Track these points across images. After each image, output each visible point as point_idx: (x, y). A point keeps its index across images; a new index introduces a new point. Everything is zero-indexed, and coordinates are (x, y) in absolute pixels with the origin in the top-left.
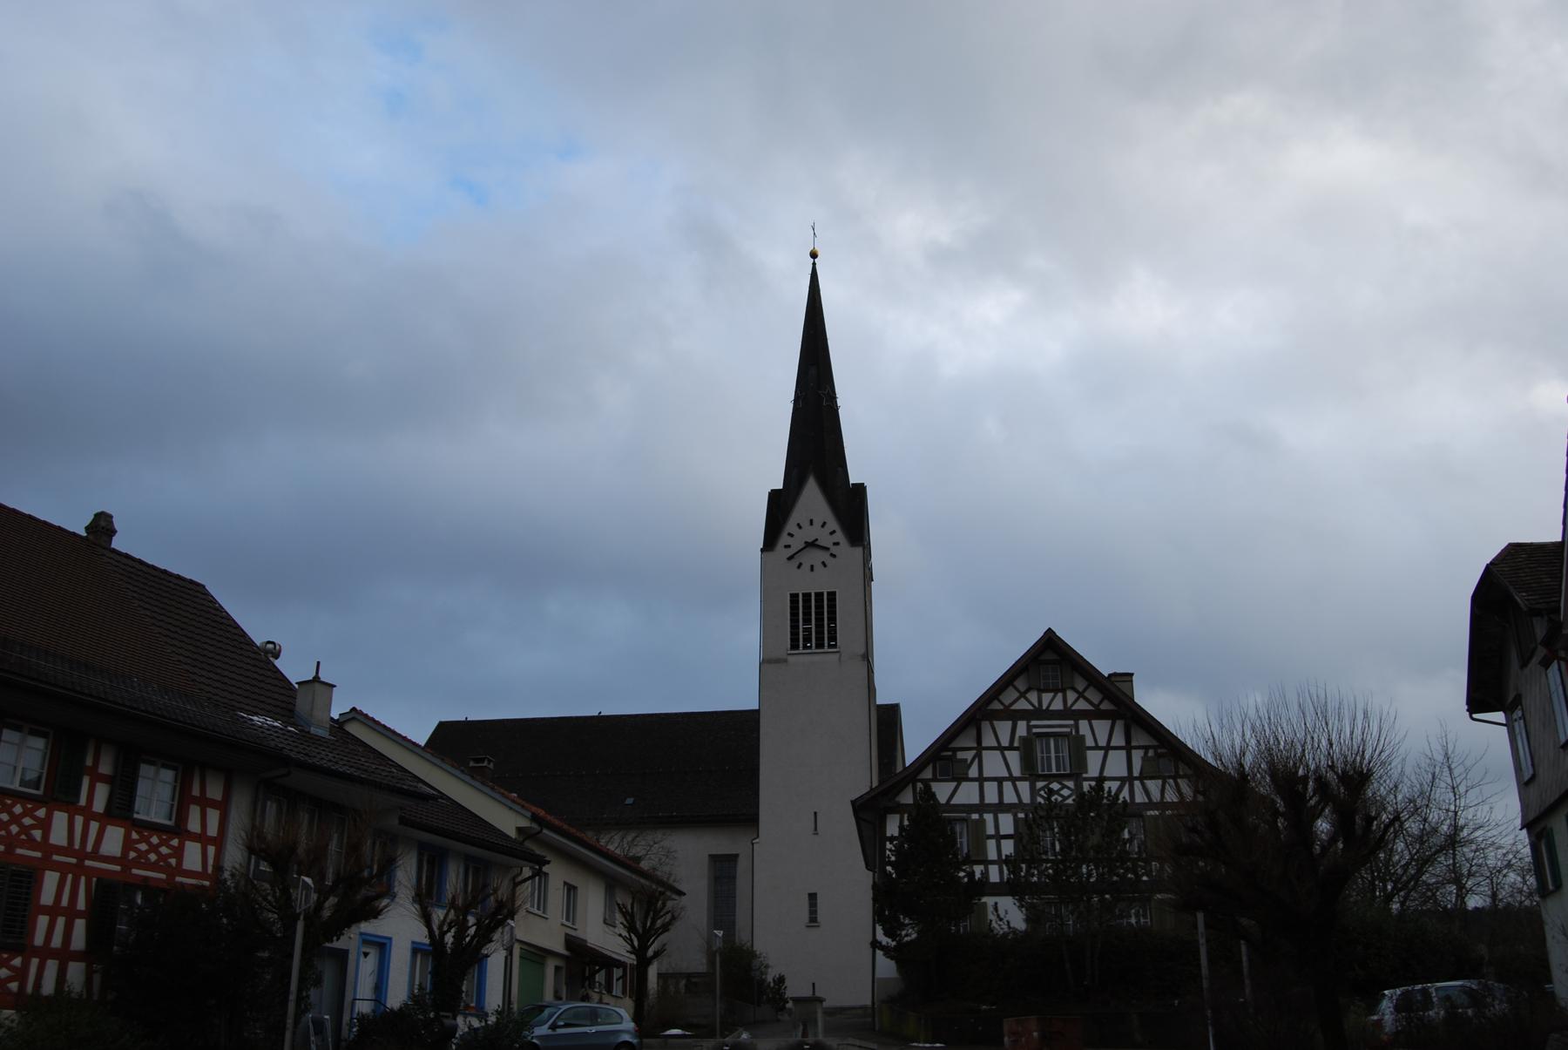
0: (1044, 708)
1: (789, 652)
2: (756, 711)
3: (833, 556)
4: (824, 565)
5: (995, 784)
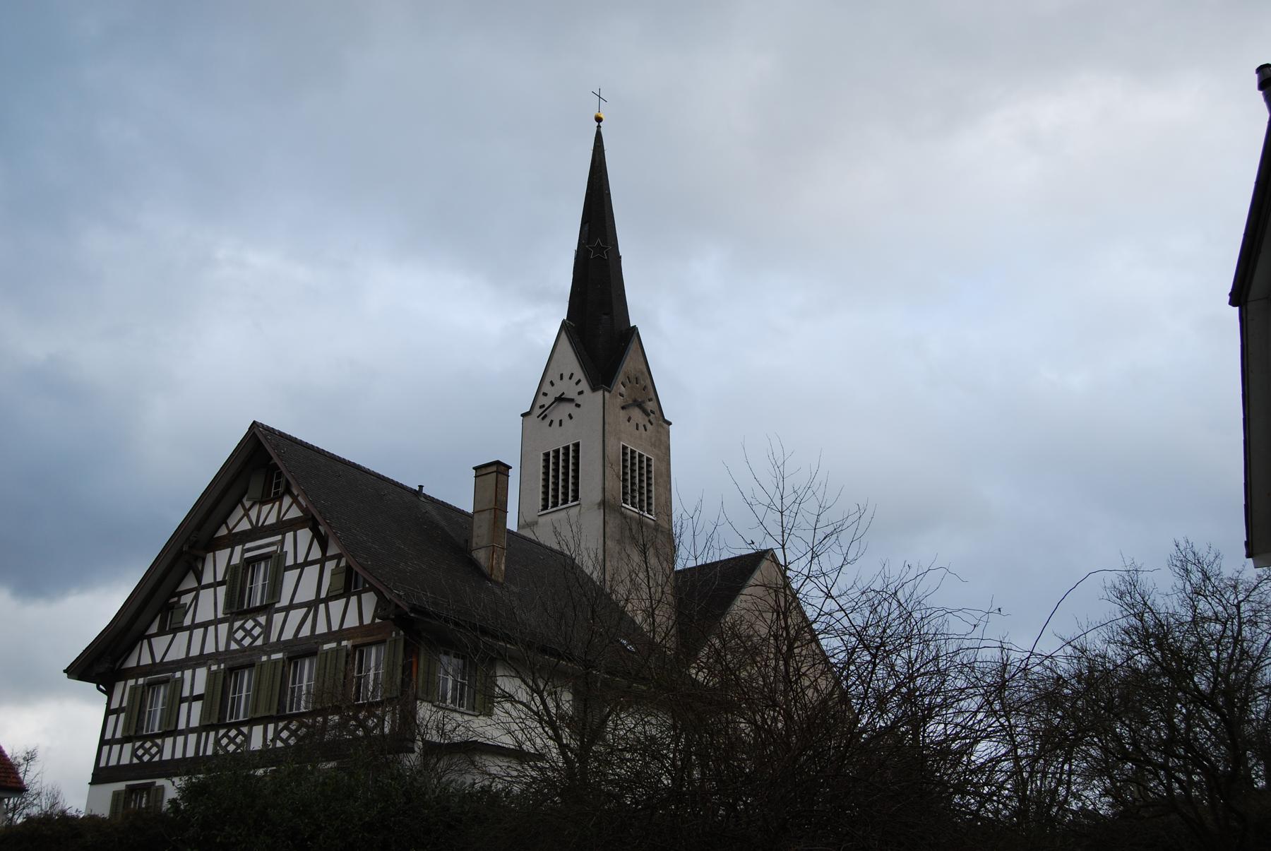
1: (539, 514)
3: (578, 406)
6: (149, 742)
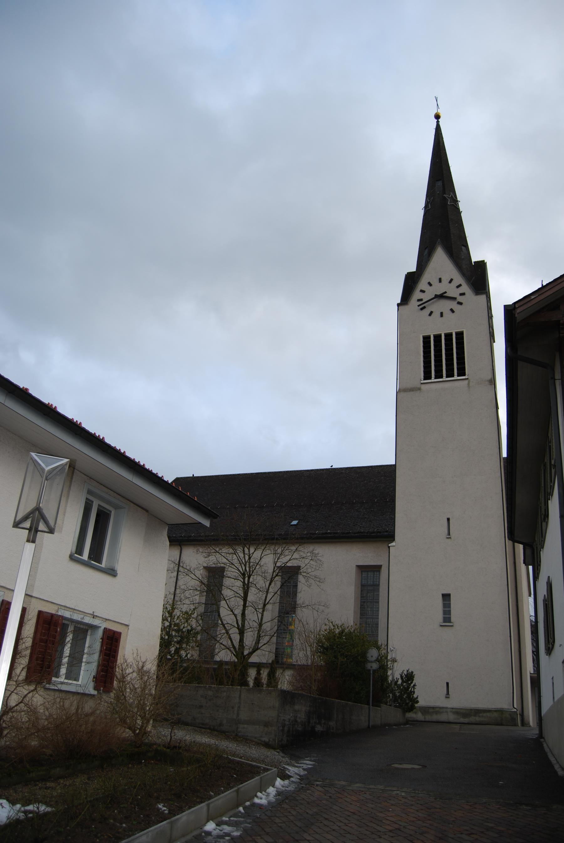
1: (422, 382)
2: (393, 465)
3: (460, 303)
4: (452, 311)
6: (316, 729)
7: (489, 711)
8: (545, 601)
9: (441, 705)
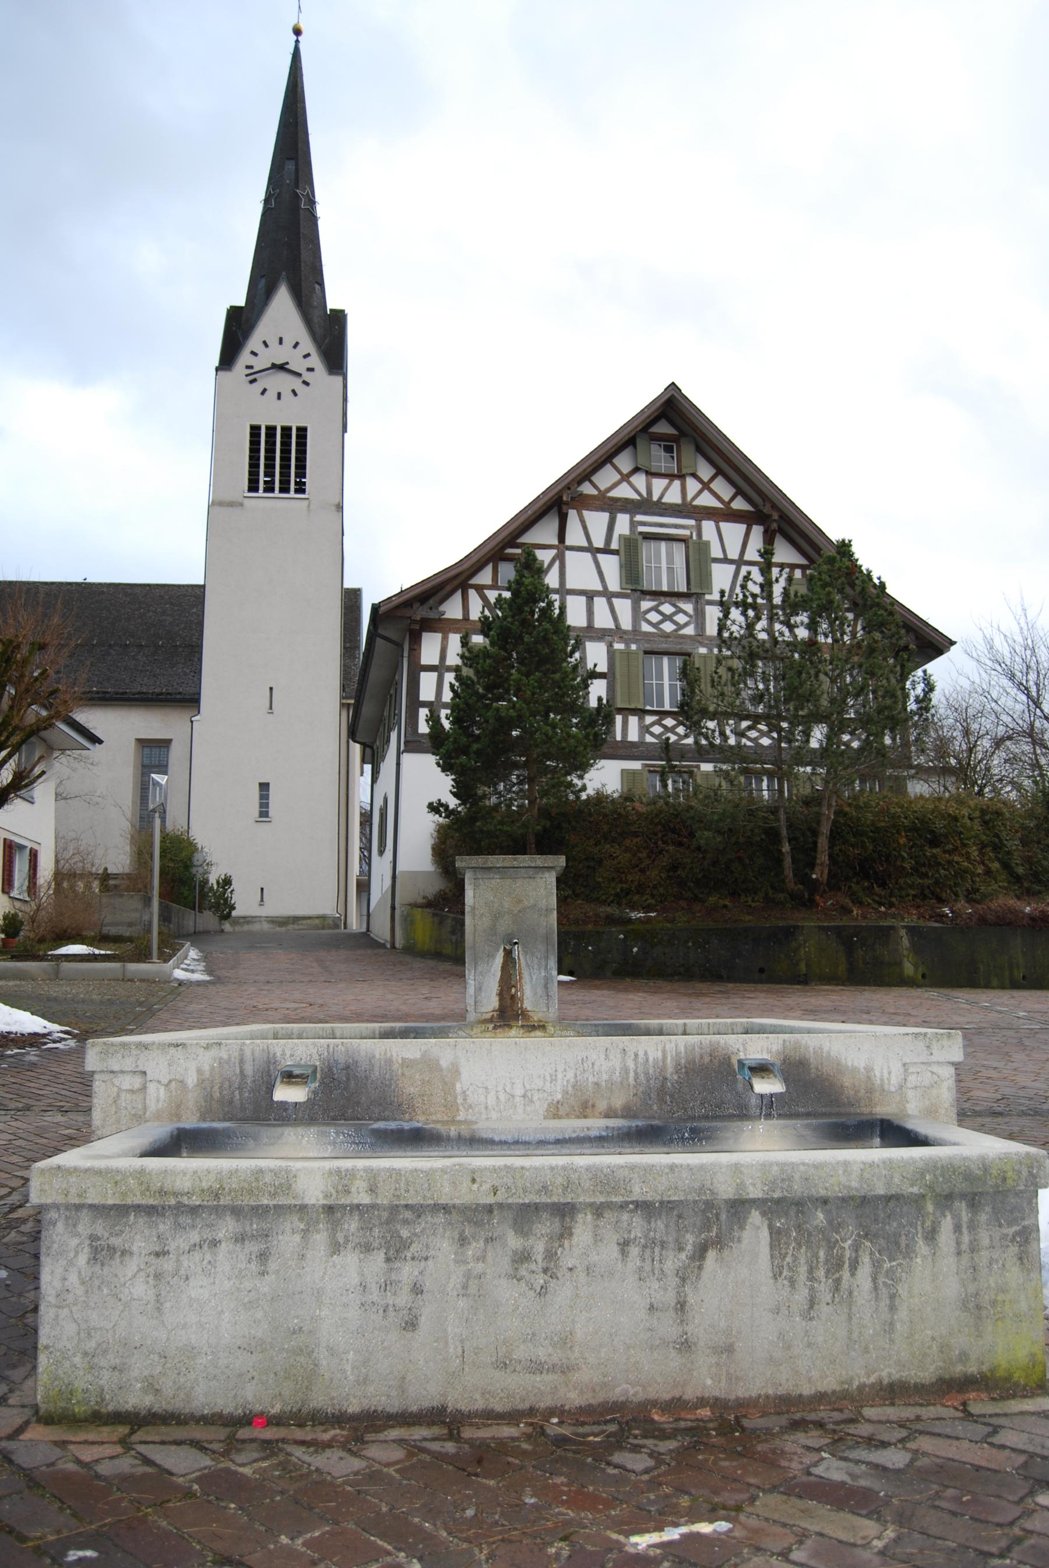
0: (655, 498)
5: (583, 599)
7: (310, 918)
8: (381, 809)
9: (254, 914)
